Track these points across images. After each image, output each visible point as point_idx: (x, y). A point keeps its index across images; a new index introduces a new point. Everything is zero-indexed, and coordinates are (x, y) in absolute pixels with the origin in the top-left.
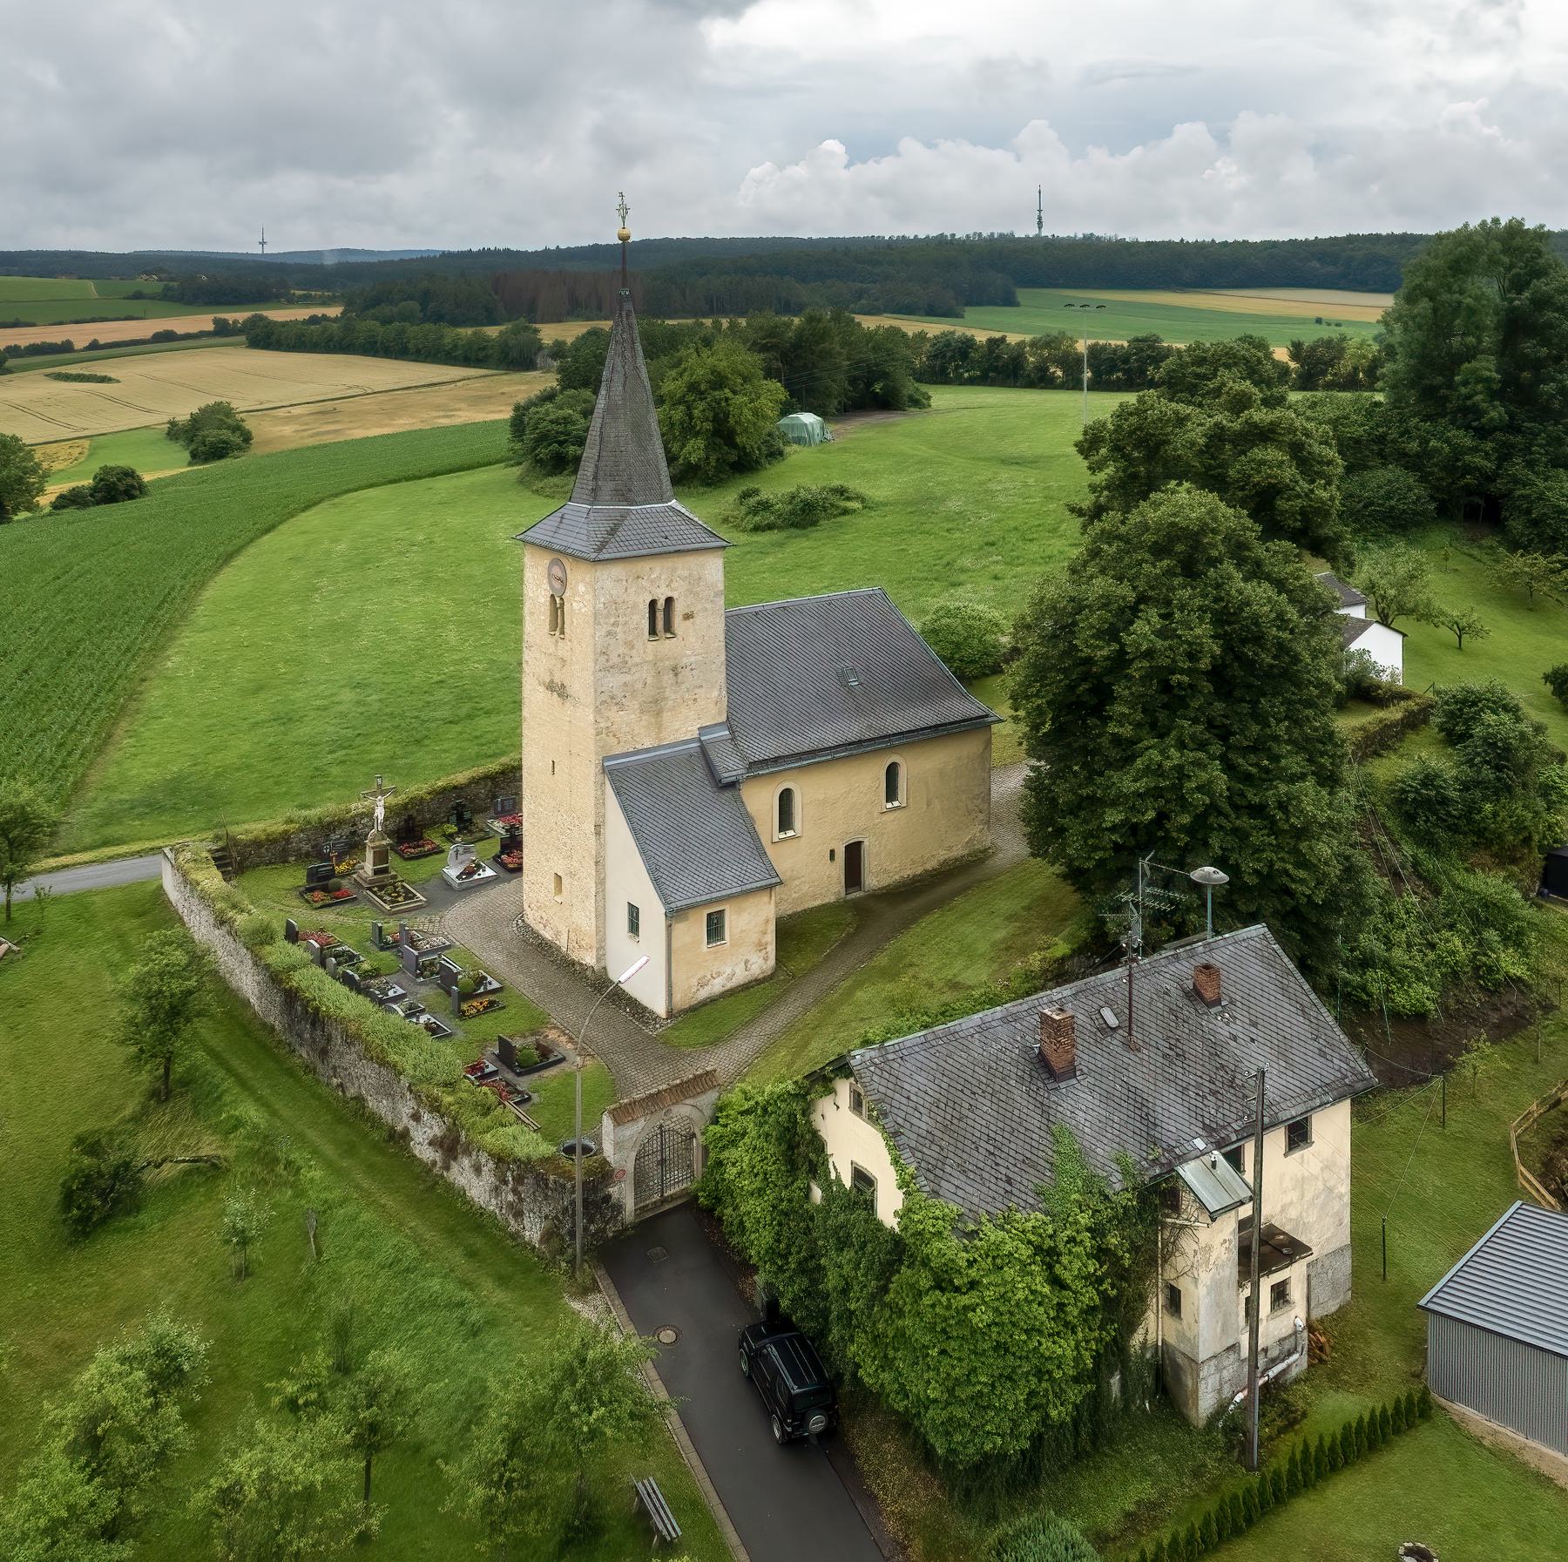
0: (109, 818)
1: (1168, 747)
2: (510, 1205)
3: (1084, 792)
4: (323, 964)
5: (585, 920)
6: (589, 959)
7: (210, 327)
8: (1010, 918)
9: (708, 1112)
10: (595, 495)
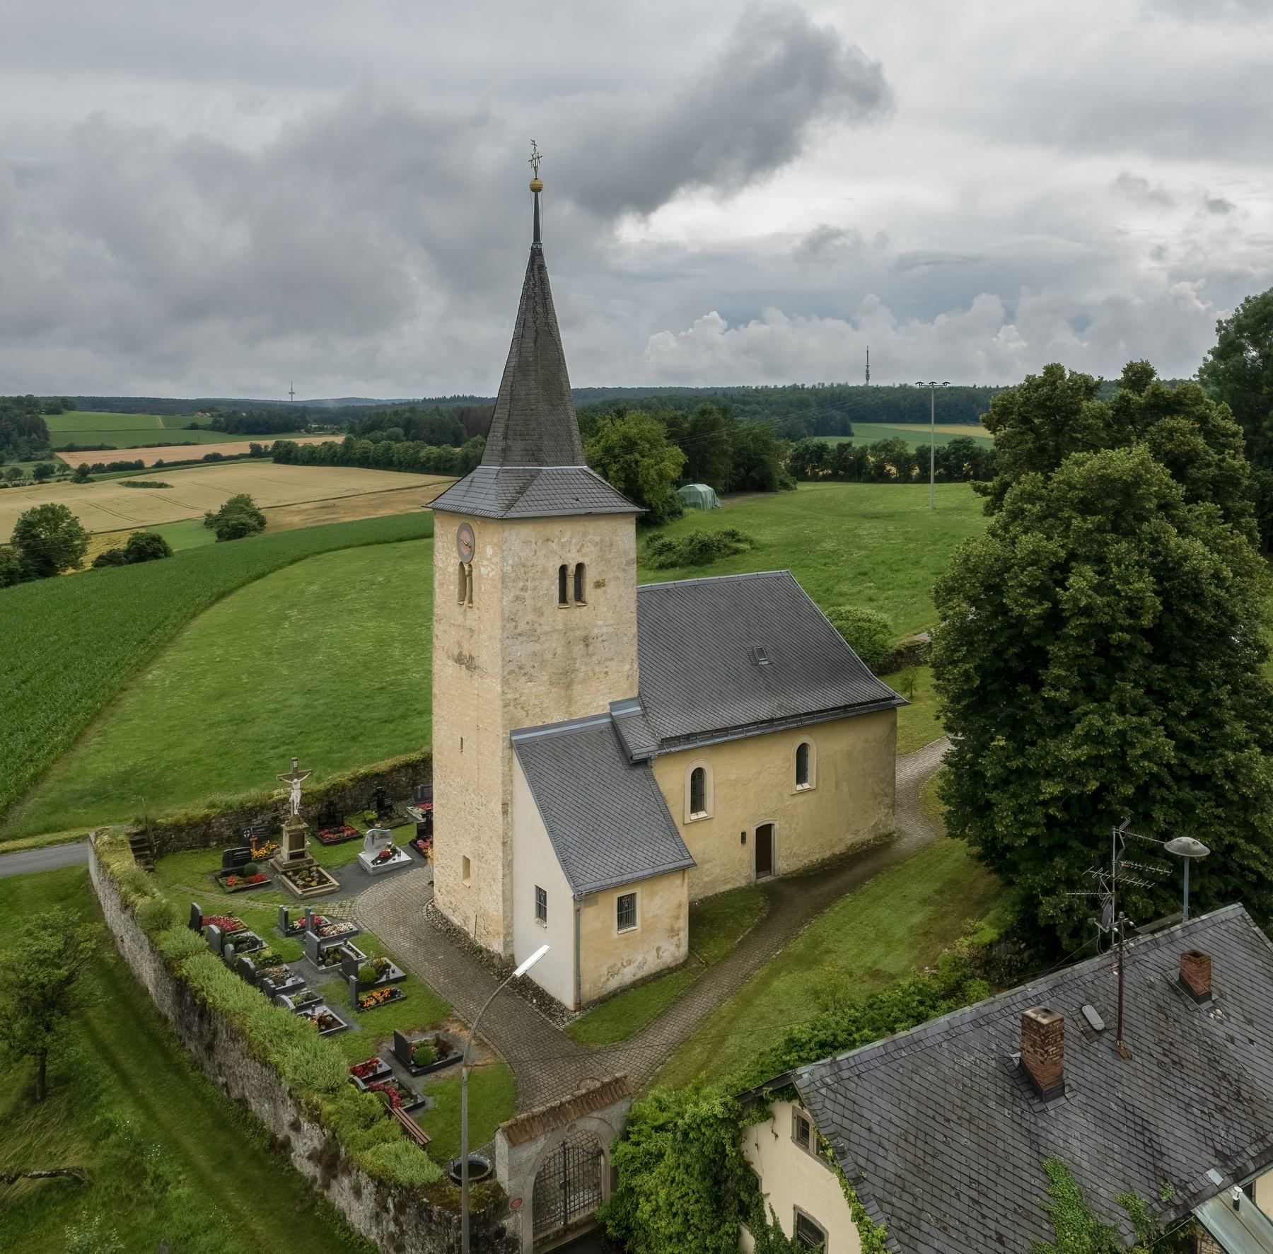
0: (57, 806)
1: (1109, 712)
2: (391, 1236)
3: (1014, 764)
4: (222, 952)
5: (495, 908)
6: (497, 946)
7: (248, 451)
8: (924, 901)
9: (618, 1126)
10: (505, 456)
